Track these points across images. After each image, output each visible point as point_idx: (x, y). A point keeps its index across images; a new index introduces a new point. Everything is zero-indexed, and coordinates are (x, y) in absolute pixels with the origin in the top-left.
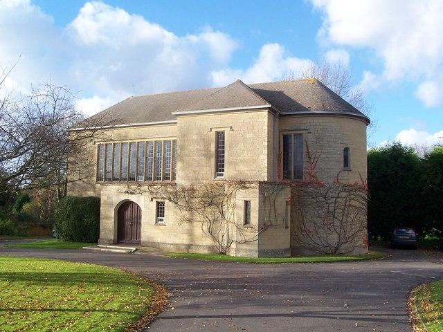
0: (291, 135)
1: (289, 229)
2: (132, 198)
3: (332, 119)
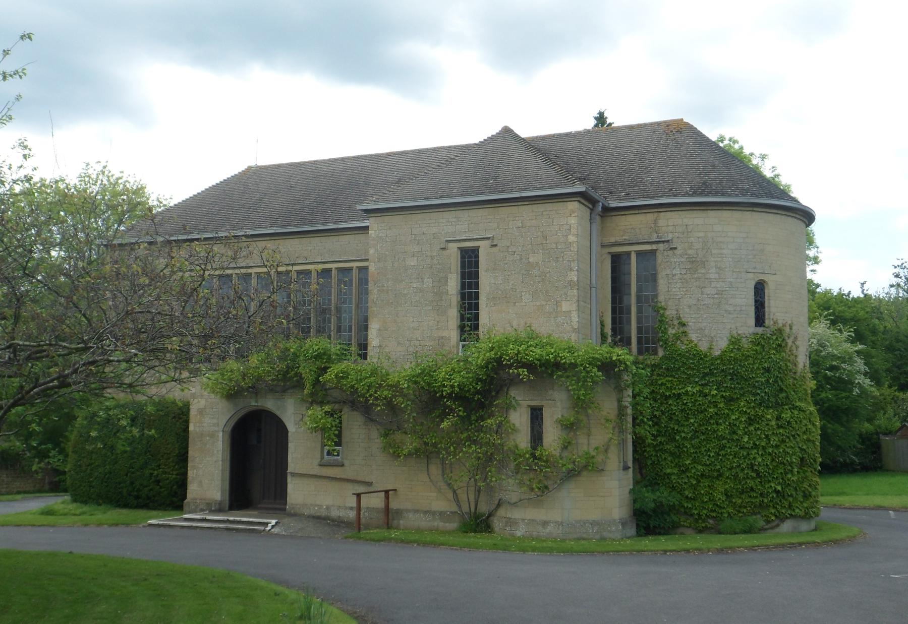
0: (628, 254)
1: (631, 470)
3: (726, 214)
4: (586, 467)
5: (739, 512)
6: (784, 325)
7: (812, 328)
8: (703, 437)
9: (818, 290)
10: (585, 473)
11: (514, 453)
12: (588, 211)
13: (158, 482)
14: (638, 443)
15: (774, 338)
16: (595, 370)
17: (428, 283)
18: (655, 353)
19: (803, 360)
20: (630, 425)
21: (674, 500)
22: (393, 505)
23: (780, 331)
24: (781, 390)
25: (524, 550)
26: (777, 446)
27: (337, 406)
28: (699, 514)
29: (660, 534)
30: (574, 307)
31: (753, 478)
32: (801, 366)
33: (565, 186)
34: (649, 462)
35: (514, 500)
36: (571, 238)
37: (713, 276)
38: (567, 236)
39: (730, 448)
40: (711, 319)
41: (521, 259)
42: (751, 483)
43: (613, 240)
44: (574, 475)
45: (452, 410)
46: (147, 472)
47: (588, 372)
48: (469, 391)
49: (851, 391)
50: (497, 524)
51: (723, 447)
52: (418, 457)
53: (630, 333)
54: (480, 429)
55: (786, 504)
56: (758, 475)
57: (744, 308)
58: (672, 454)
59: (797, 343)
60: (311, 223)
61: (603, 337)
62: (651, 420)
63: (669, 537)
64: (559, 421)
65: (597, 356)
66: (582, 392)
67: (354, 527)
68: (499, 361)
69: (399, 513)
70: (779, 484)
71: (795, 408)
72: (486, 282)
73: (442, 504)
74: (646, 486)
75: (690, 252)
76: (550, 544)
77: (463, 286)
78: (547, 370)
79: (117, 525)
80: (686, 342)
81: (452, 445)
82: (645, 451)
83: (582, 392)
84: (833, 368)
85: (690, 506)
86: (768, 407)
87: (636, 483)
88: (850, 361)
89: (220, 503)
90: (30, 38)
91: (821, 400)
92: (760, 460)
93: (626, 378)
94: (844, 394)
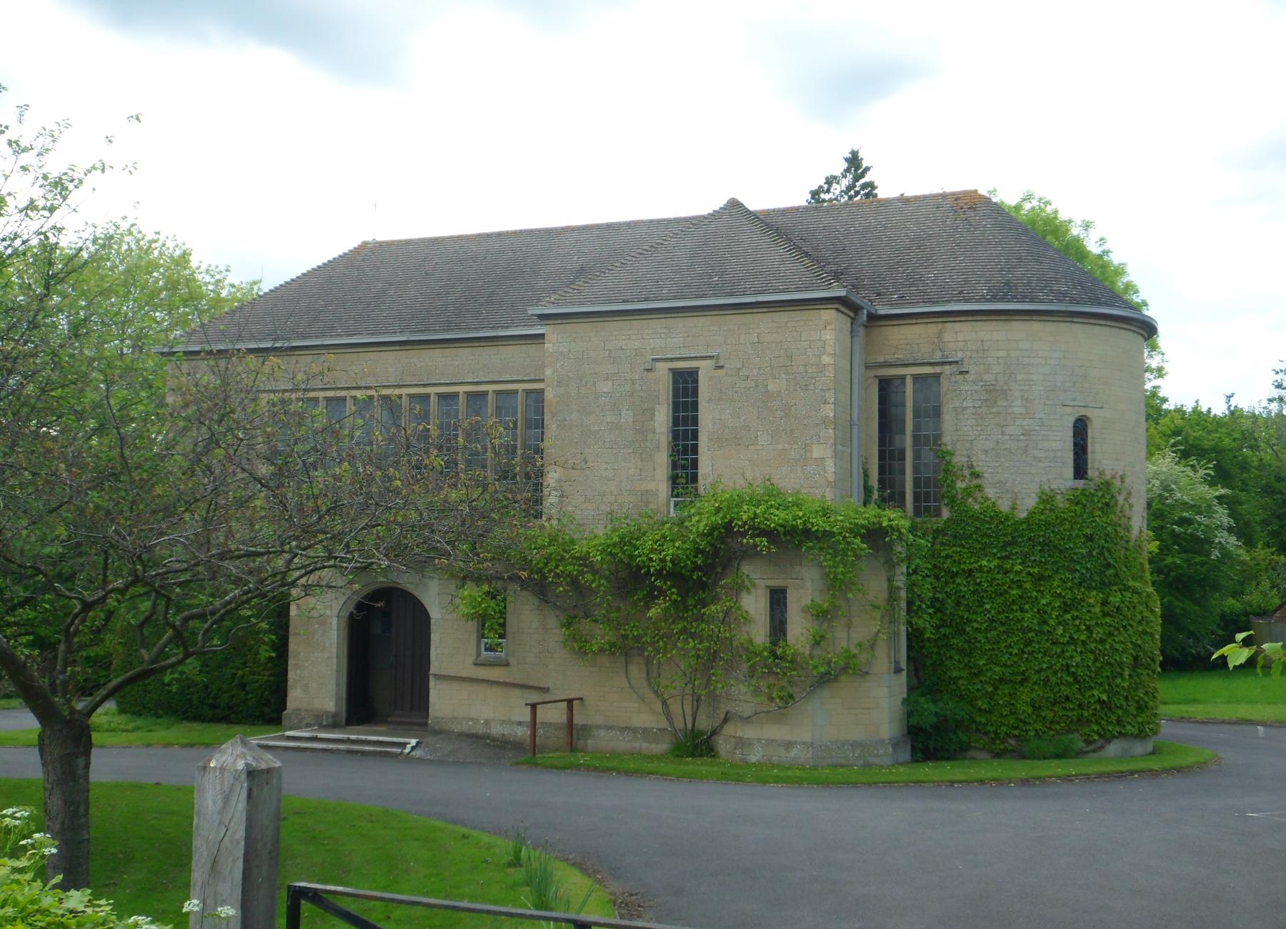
0: (903, 378)
1: (904, 673)
2: (406, 581)
3: (1036, 326)
4: (845, 669)
5: (1050, 729)
6: (1113, 477)
7: (1153, 464)
8: (1002, 629)
9: (1165, 406)
10: (843, 678)
11: (747, 650)
12: (849, 320)
13: (243, 686)
14: (915, 638)
15: (1100, 494)
16: (858, 540)
17: (627, 416)
18: (938, 513)
19: (1138, 522)
20: (903, 613)
21: (963, 713)
22: (578, 720)
23: (1108, 484)
24: (1109, 565)
25: (764, 782)
26: (1102, 641)
27: (499, 585)
28: (995, 732)
29: (943, 759)
30: (830, 453)
31: (1069, 684)
32: (1135, 532)
33: (818, 289)
34: (929, 662)
35: (746, 714)
36: (826, 359)
37: (1017, 410)
38: (819, 356)
39: (1039, 643)
40: (1012, 466)
41: (757, 386)
42: (1066, 691)
43: (881, 359)
44: (828, 680)
45: (662, 592)
46: (228, 671)
47: (848, 543)
48: (685, 567)
49: (1209, 554)
50: (723, 746)
51: (1029, 643)
52: (613, 654)
53: (903, 486)
54: (700, 618)
55: (1114, 718)
56: (1075, 679)
57: (1059, 454)
58: (960, 651)
59: (1132, 500)
60: (458, 327)
61: (867, 490)
62: (932, 606)
63: (956, 763)
64: (806, 610)
65: (861, 522)
66: (840, 570)
67: (524, 752)
68: (728, 526)
69: (586, 729)
70: (1105, 691)
71: (1127, 588)
72: (708, 417)
73: (647, 718)
74: (924, 695)
75: (986, 377)
76: (797, 773)
77: (676, 421)
78: (792, 540)
79: (192, 745)
80: (980, 500)
81: (662, 638)
82: (923, 647)
83: (840, 570)
84: (1183, 522)
85: (983, 720)
86: (1089, 588)
87: (911, 689)
88: (1209, 511)
89: (335, 715)
90: (138, 119)
91: (1166, 566)
92: (1078, 659)
93: (899, 549)
94: (1198, 559)
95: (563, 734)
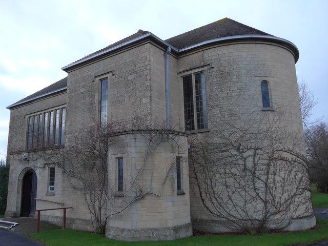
3: (240, 46)
12: (163, 53)
37: (235, 80)
43: (183, 70)
89: (15, 213)
95: (62, 221)
